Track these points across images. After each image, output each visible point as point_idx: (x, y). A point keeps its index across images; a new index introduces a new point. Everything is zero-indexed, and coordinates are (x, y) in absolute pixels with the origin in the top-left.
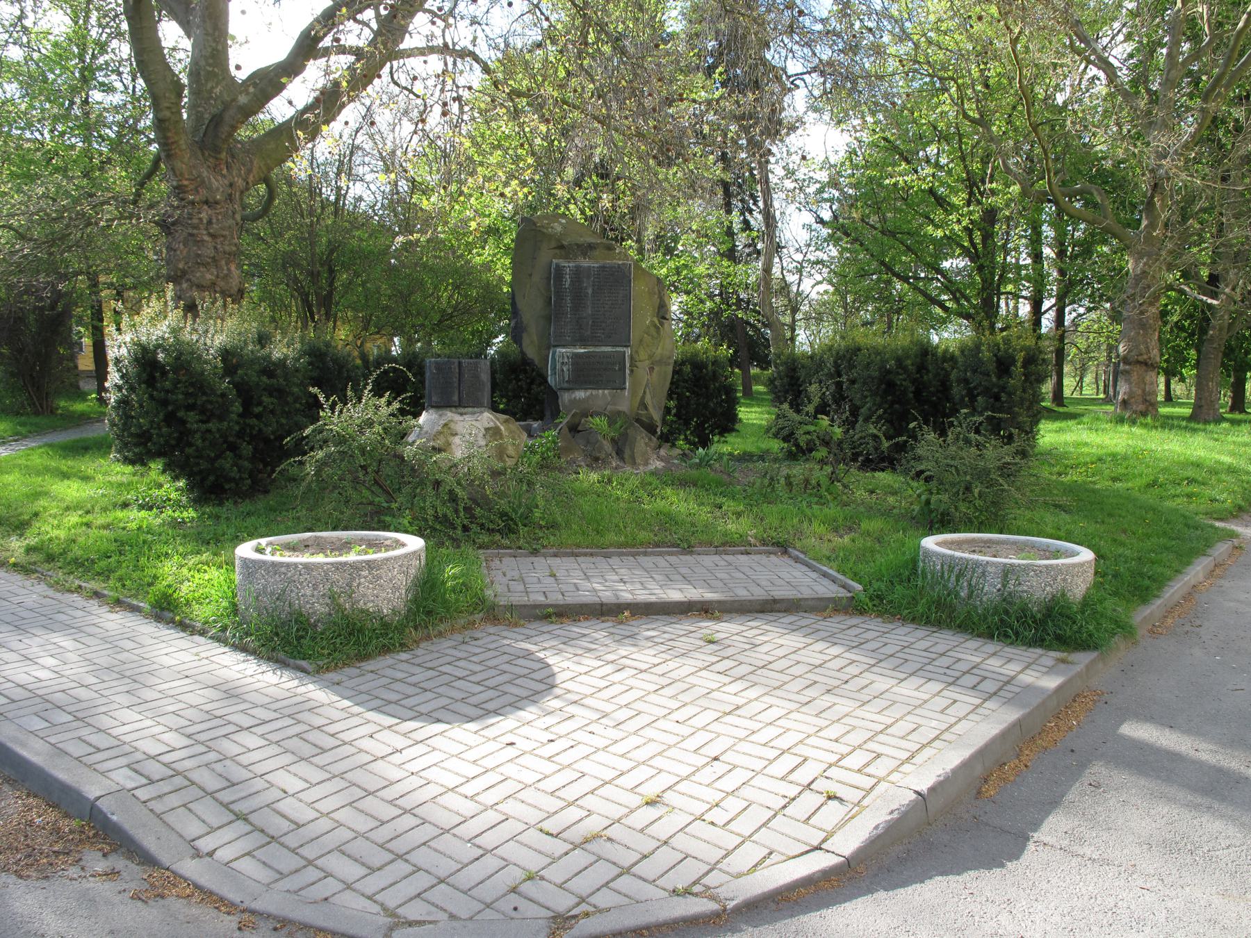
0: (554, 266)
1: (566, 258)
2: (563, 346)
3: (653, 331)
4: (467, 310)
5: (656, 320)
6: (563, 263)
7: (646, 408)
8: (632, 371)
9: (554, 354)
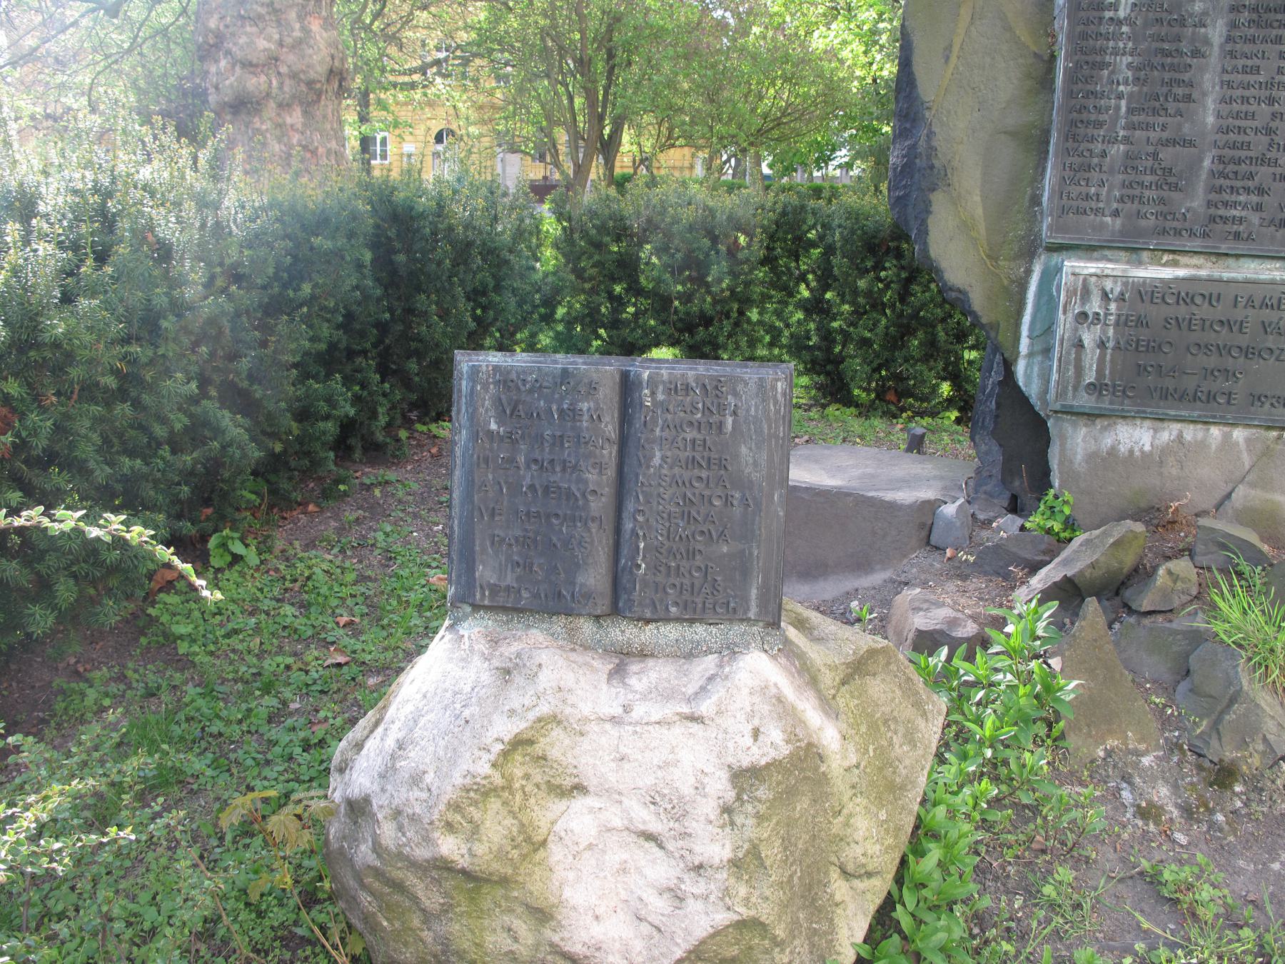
2: (1089, 250)
4: (801, 115)
9: (1050, 275)
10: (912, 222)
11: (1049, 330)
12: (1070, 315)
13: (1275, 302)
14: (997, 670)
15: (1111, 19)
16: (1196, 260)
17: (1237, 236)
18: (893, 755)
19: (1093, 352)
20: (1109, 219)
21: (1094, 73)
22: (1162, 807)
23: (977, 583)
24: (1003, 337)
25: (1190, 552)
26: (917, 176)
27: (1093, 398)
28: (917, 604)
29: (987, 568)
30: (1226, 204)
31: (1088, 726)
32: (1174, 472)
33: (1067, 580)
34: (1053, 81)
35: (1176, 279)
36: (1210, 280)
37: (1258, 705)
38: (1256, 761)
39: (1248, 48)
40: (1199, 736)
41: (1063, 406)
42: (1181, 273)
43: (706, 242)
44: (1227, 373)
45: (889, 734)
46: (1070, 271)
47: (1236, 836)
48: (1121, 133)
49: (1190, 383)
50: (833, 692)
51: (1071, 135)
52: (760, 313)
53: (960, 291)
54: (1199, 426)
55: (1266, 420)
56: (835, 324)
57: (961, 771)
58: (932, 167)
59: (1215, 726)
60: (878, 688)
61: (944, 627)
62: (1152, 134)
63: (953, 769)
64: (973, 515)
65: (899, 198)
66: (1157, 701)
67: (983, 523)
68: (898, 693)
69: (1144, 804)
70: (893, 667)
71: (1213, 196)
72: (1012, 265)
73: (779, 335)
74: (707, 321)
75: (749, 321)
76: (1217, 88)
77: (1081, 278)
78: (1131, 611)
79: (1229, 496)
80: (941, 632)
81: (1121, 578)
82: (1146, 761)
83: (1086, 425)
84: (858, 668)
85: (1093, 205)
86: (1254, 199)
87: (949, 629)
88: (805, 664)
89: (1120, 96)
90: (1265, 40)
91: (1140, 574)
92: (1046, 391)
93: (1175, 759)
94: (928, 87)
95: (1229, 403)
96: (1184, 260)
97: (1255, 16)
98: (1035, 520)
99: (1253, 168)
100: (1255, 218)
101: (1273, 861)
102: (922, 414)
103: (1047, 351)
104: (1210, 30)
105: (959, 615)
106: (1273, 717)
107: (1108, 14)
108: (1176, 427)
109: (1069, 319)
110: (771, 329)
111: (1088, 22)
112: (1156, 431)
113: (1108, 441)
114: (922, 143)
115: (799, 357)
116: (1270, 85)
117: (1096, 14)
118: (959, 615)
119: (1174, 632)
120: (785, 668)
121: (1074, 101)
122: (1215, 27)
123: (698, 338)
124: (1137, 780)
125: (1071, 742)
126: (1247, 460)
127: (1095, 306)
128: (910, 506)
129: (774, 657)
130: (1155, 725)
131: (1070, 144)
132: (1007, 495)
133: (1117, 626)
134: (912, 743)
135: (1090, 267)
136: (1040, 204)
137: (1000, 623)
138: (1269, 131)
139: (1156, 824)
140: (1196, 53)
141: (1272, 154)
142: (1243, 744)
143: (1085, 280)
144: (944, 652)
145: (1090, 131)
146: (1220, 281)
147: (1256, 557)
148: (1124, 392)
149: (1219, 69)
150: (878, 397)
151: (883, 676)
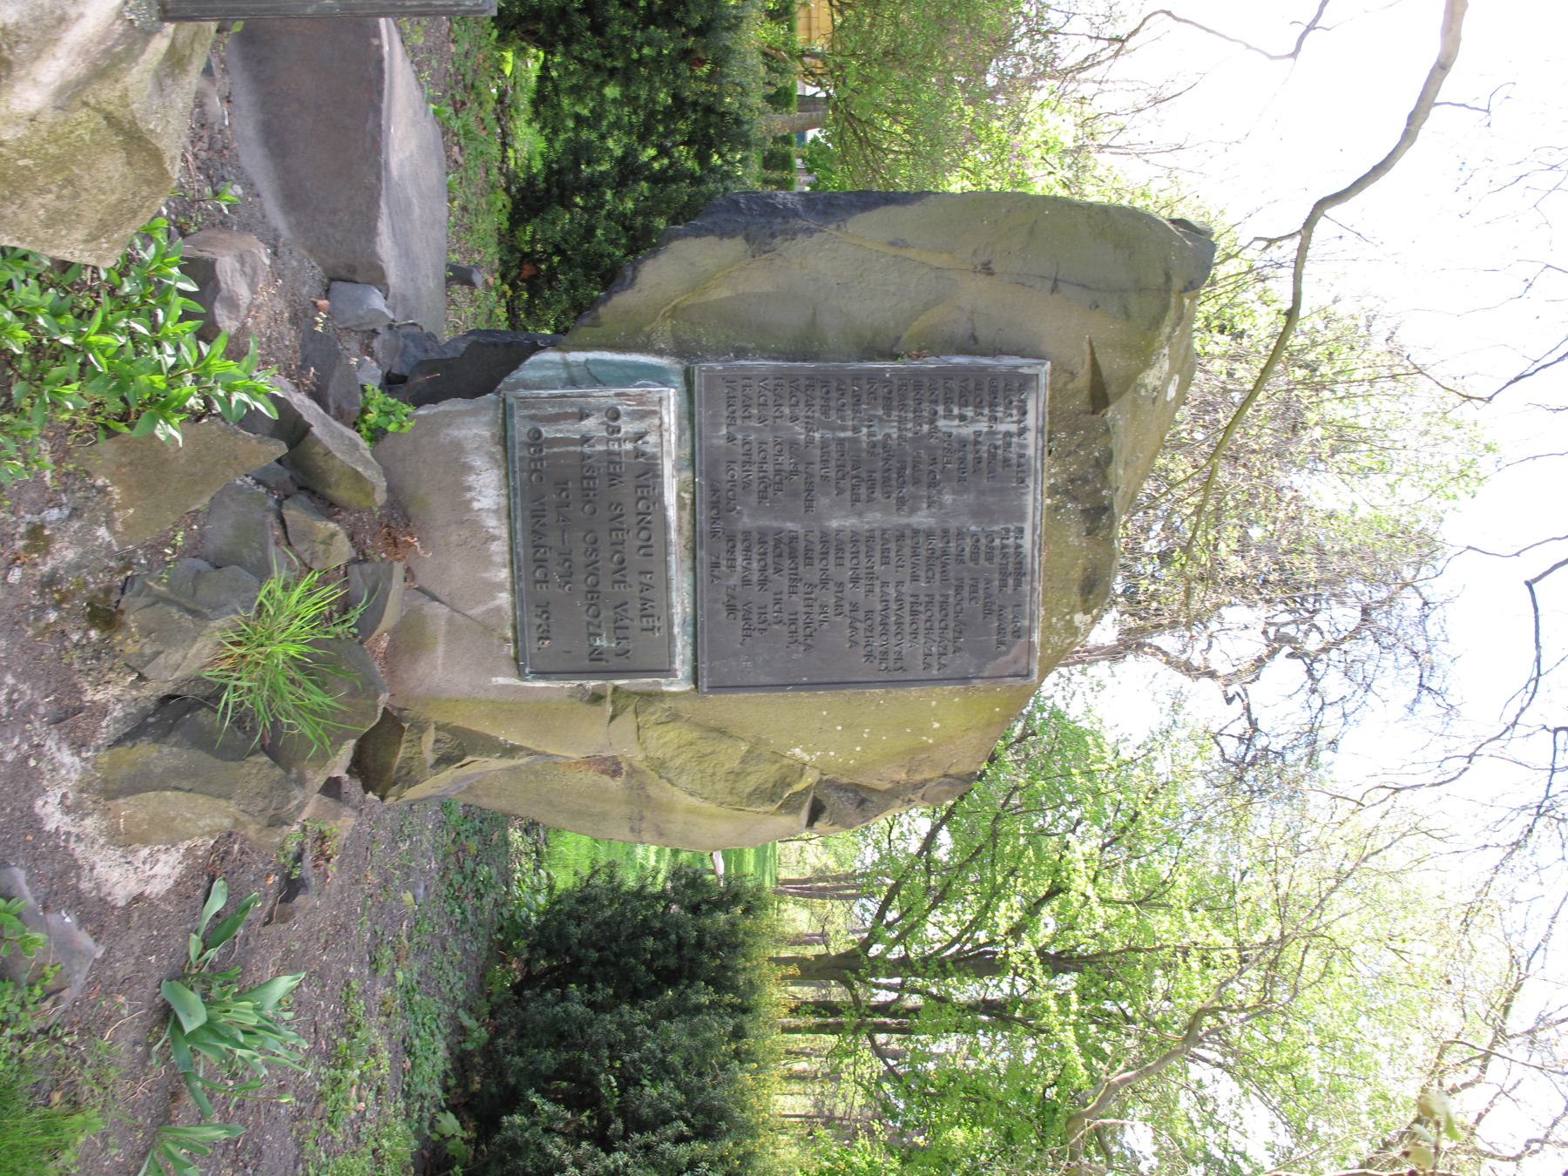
0: (1025, 366)
1: (1056, 417)
2: (689, 416)
3: (763, 774)
5: (810, 779)
6: (1036, 408)
7: (445, 760)
8: (597, 698)
9: (659, 376)
10: (710, 220)
11: (596, 381)
12: (615, 401)
13: (649, 611)
14: (178, 348)
16: (687, 527)
17: (716, 565)
18: (27, 195)
19: (574, 432)
20: (724, 431)
21: (880, 401)
22: (48, 553)
23: (290, 336)
24: (584, 332)
25: (361, 558)
26: (763, 220)
27: (525, 438)
28: (248, 260)
29: (310, 347)
30: (748, 550)
31: (131, 463)
32: (454, 538)
33: (305, 429)
34: (871, 359)
35: (664, 509)
36: (666, 543)
37: (195, 640)
38: (131, 648)
39: (907, 551)
40: (145, 585)
41: (512, 406)
42: (672, 513)
43: (696, 20)
44: (568, 576)
45: (54, 188)
46: (664, 395)
47: (35, 636)
48: (817, 435)
49: (552, 539)
50: (92, 101)
51: (813, 381)
52: (614, 101)
53: (634, 279)
54: (507, 557)
55: (522, 624)
56: (609, 195)
57: (36, 308)
58: (773, 236)
59: (160, 599)
60: (112, 168)
61: (224, 293)
62: (817, 467)
63: (35, 298)
64: (375, 333)
65: (737, 203)
66: (179, 538)
67: (368, 346)
68: (114, 198)
69: (47, 532)
70: (145, 190)
71: (755, 536)
72: (668, 334)
73: (590, 127)
74: (598, 28)
75: (603, 84)
78: (280, 503)
79: (435, 599)
80: (217, 289)
81: (319, 489)
82: (102, 532)
83: (493, 435)
84: (134, 140)
86: (755, 577)
87: (222, 299)
88: (121, 61)
89: (856, 429)
90: (914, 565)
91: (329, 507)
92: (527, 387)
93: (112, 564)
94: (867, 227)
95: (537, 582)
96: (686, 515)
97: (938, 553)
98: (378, 397)
99: (786, 572)
100: (735, 580)
101: (14, 676)
102: (510, 309)
103: (572, 382)
104: (925, 512)
105: (243, 312)
106: (185, 657)
107: (941, 409)
108: (503, 532)
110: (598, 115)
111: (932, 390)
112: (496, 511)
113: (478, 462)
114: (800, 223)
115: (564, 153)
116: (871, 576)
117: (941, 396)
118: (243, 312)
119: (264, 548)
120: (108, 31)
121: (849, 382)
123: (576, 17)
124: (76, 525)
125: (107, 447)
126: (476, 611)
127: (627, 427)
128: (374, 253)
129: (120, 15)
130: (149, 538)
131: (803, 382)
132: (406, 372)
133: (262, 490)
134: (50, 223)
135: (670, 416)
136: (737, 357)
137: (235, 352)
138: (824, 583)
139: (25, 548)
140: (901, 502)
141: (801, 587)
142: (146, 632)
143: (655, 412)
144: (192, 287)
145: (818, 402)
146: (667, 554)
147: (367, 626)
148: (536, 470)
149: (885, 526)
150: (525, 255)
151: (131, 177)
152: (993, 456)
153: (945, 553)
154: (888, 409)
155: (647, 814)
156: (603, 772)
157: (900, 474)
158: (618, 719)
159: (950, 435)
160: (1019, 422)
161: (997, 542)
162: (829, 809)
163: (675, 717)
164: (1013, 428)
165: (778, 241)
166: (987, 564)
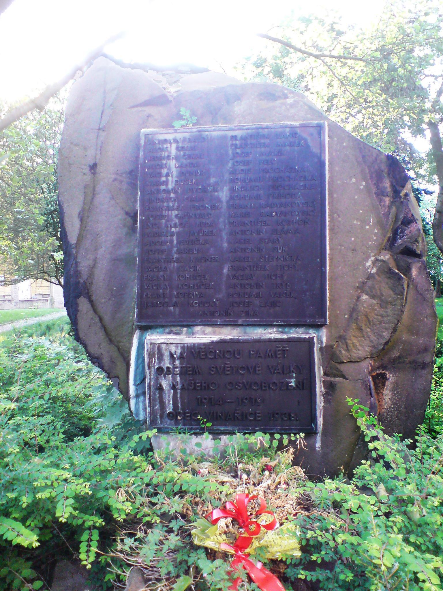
5: (386, 256)
15: (164, 190)
19: (169, 393)
46: (149, 342)
48: (175, 256)
71: (231, 290)
76: (227, 226)
77: (157, 346)
85: (162, 300)
89: (172, 235)
100: (257, 302)
107: (163, 187)
109: (152, 373)
122: (223, 191)
127: (167, 363)
152: (189, 157)
153: (243, 181)
154: (162, 217)
155: (411, 358)
156: (384, 385)
157: (198, 208)
158: (345, 373)
159: (177, 181)
160: (171, 143)
161: (238, 151)
162: (409, 245)
163: (341, 338)
164: (174, 146)
165: (81, 280)
166: (251, 156)
